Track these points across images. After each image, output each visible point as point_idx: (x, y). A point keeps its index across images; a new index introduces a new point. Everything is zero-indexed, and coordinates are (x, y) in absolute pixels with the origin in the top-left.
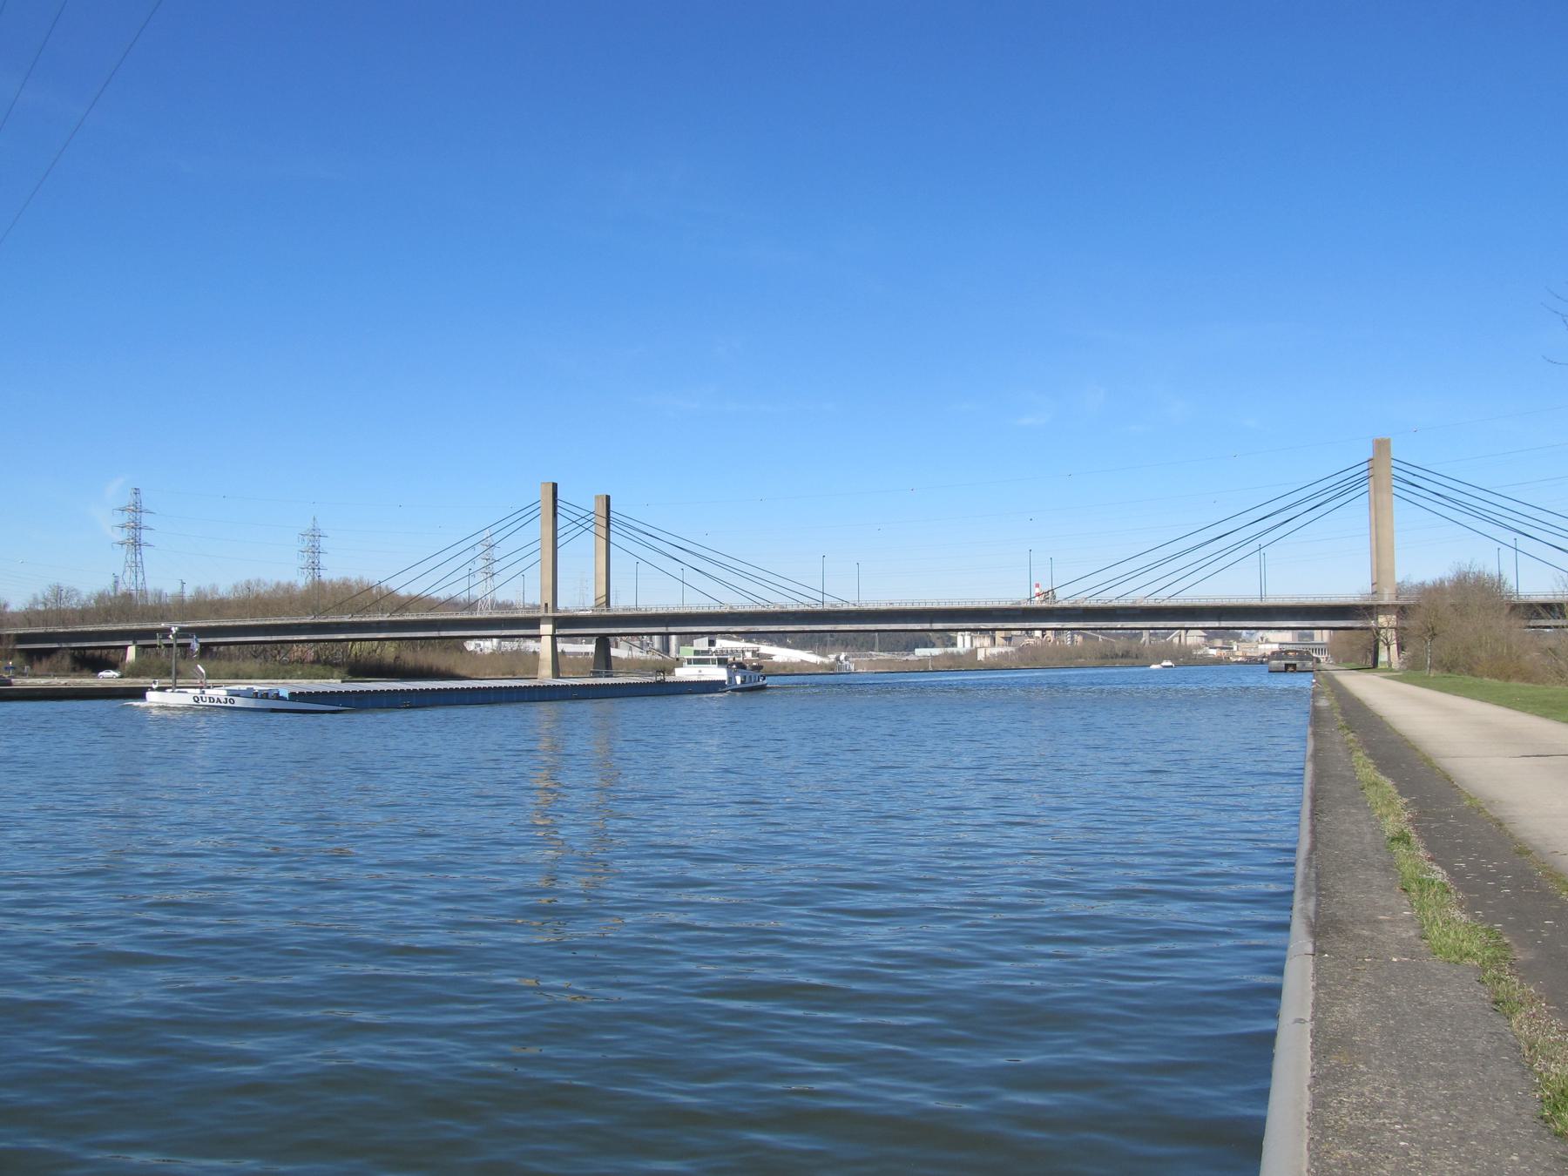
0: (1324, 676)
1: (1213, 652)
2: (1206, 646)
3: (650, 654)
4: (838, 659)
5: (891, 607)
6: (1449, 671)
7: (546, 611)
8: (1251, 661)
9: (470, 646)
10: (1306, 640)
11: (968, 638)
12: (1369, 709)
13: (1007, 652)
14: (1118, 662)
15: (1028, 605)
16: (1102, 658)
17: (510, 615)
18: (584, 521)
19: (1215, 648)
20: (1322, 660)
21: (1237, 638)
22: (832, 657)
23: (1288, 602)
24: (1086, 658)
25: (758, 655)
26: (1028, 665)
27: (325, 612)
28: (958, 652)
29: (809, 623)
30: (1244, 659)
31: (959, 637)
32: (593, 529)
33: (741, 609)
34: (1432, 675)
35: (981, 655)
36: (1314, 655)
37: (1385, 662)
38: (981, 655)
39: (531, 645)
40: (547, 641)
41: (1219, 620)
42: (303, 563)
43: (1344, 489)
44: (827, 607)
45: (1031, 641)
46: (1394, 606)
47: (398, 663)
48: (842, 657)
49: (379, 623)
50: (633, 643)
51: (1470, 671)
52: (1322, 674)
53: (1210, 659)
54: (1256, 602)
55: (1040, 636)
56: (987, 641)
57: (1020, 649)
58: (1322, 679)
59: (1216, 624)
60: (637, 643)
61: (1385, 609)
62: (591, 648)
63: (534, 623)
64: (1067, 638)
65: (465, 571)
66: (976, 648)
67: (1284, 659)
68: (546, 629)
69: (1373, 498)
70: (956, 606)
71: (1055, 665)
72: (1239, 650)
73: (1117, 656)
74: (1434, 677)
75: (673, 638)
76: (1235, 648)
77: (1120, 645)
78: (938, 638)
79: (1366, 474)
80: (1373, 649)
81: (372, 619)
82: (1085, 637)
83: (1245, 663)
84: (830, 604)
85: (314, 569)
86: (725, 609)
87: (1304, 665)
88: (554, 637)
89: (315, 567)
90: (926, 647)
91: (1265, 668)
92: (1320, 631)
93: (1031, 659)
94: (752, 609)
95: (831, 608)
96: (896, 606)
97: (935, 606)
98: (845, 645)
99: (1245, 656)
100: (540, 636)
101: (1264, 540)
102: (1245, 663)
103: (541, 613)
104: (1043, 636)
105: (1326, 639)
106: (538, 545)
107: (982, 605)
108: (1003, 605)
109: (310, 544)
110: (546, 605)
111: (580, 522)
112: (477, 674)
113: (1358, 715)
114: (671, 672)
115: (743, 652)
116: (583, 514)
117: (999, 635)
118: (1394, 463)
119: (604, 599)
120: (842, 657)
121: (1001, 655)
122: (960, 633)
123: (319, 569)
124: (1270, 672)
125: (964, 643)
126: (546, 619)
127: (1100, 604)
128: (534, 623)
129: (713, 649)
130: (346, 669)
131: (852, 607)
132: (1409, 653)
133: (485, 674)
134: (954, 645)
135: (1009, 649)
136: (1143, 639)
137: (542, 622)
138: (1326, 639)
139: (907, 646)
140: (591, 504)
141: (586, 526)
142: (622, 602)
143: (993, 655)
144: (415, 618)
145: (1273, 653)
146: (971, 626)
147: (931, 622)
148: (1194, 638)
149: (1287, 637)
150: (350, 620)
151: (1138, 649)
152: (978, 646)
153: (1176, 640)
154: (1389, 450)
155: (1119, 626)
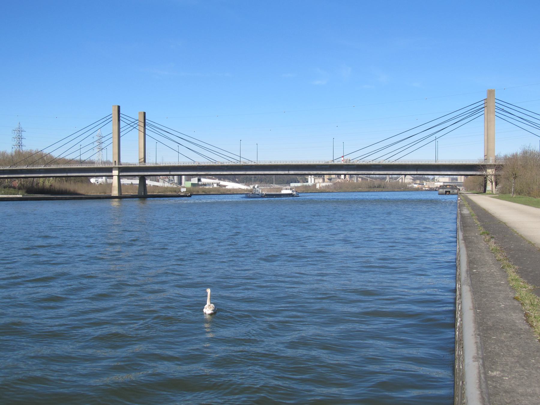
0: (463, 196)
1: (416, 186)
2: (413, 183)
3: (172, 185)
4: (254, 187)
5: (270, 164)
6: (519, 194)
7: (115, 164)
8: (431, 190)
9: (93, 180)
10: (455, 181)
11: (313, 179)
12: (524, 239)
13: (329, 185)
14: (375, 189)
15: (332, 163)
16: (369, 188)
17: (92, 166)
18: (133, 124)
19: (416, 184)
20: (461, 189)
21: (426, 180)
22: (252, 187)
23: (447, 163)
24: (362, 188)
25: (220, 185)
26: (337, 190)
27: (33, 163)
28: (309, 185)
29: (234, 171)
30: (428, 189)
31: (309, 178)
32: (138, 128)
33: (203, 164)
34: (514, 196)
35: (318, 186)
36: (458, 187)
37: (489, 190)
38: (318, 186)
39: (109, 181)
40: (115, 179)
41: (417, 171)
42: (14, 143)
43: (474, 112)
44: (242, 163)
45: (340, 180)
46: (495, 165)
47: (52, 188)
48: (256, 187)
49: (40, 169)
50: (165, 180)
51: (529, 194)
52: (462, 195)
53: (414, 188)
54: (433, 163)
55: (343, 178)
56: (321, 180)
57: (335, 184)
58: (462, 198)
59: (415, 173)
60: (167, 180)
61: (490, 166)
62: (136, 181)
63: (110, 170)
64: (355, 179)
65: (78, 147)
66: (316, 183)
67: (445, 189)
68: (115, 173)
69: (486, 117)
70: (300, 163)
71: (349, 191)
72: (427, 185)
73: (375, 187)
74: (515, 197)
75: (183, 177)
76: (425, 184)
77: (377, 183)
78: (301, 179)
79: (483, 106)
80: (483, 184)
81: (36, 168)
82: (362, 178)
83: (429, 190)
84: (243, 162)
85: (19, 146)
86: (196, 164)
87: (453, 191)
88: (119, 177)
89: (20, 145)
90: (295, 182)
91: (437, 193)
92: (460, 176)
93: (339, 188)
94: (208, 164)
95: (244, 164)
96: (273, 163)
97: (291, 163)
98: (261, 181)
99: (429, 188)
100: (112, 176)
101: (438, 135)
102: (429, 190)
103: (113, 165)
104: (345, 178)
105: (462, 181)
106: (111, 136)
107: (312, 163)
108: (321, 163)
109: (18, 135)
110: (115, 161)
111: (132, 125)
112: (88, 193)
113: (475, 207)
114: (281, 191)
115: (213, 184)
116: (133, 120)
117: (326, 177)
118: (496, 101)
119: (143, 160)
120: (256, 187)
121: (326, 186)
122: (309, 176)
123: (22, 146)
124: (439, 194)
125: (311, 180)
126: (115, 168)
127: (364, 163)
128: (110, 170)
129: (200, 183)
130: (25, 190)
131: (253, 164)
132: (500, 186)
133: (92, 193)
134: (307, 182)
135: (330, 184)
136: (387, 180)
137: (113, 169)
138: (462, 181)
139: (287, 182)
140: (138, 116)
141: (134, 126)
142: (151, 162)
143: (323, 186)
144: (56, 167)
145: (440, 186)
146: (315, 172)
147: (289, 171)
148: (408, 179)
149: (446, 179)
150: (26, 168)
151: (384, 184)
152: (317, 182)
153: (400, 181)
154: (494, 95)
155: (372, 173)
